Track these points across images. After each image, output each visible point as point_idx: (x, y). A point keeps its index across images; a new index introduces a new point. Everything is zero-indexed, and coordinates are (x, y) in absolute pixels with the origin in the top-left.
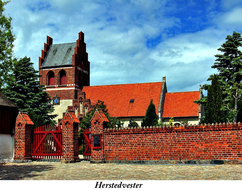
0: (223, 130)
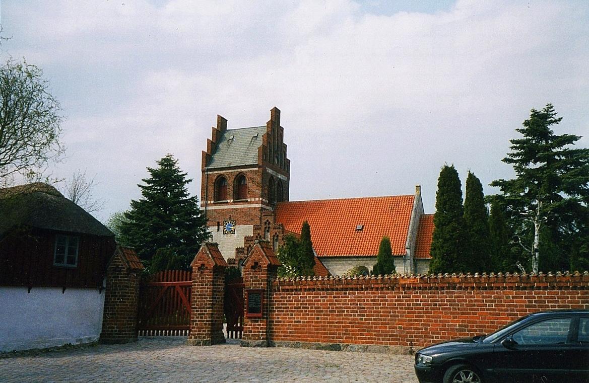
0: (498, 288)
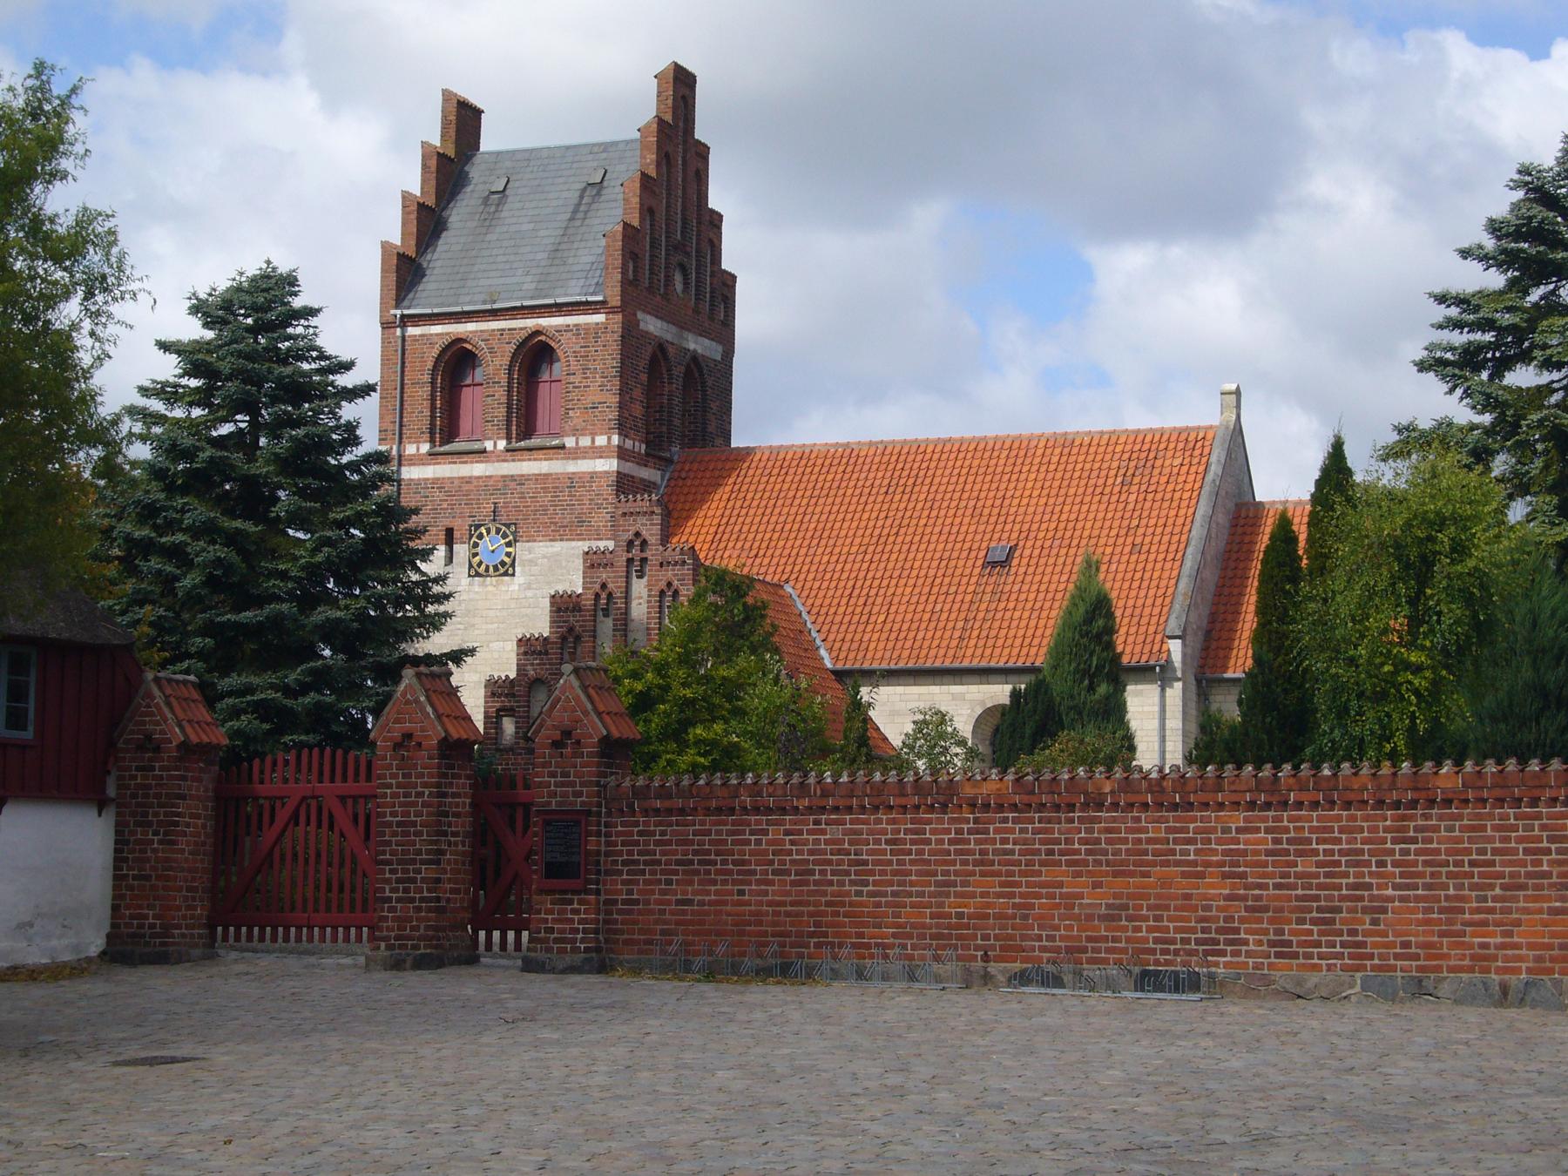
0: (1205, 806)
